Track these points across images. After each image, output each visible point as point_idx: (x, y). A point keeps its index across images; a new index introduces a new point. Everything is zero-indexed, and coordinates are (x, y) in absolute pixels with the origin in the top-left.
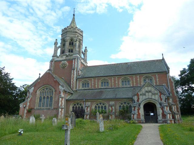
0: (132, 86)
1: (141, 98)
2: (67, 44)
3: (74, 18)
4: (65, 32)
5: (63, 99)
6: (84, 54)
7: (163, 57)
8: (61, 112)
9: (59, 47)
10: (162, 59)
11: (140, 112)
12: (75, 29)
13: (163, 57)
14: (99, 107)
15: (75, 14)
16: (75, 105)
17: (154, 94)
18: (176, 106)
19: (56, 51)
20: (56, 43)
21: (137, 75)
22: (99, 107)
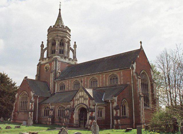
0: (98, 86)
1: (76, 103)
2: (57, 43)
3: (60, 13)
4: (51, 30)
5: (33, 103)
6: (74, 52)
7: (141, 46)
8: (31, 114)
9: (46, 49)
10: (139, 48)
11: (74, 116)
12: (56, 27)
13: (141, 46)
14: (61, 110)
15: (61, 9)
16: (46, 108)
17: (85, 99)
18: (34, 114)
19: (42, 54)
20: (42, 46)
21: (85, 77)
22: (61, 110)
